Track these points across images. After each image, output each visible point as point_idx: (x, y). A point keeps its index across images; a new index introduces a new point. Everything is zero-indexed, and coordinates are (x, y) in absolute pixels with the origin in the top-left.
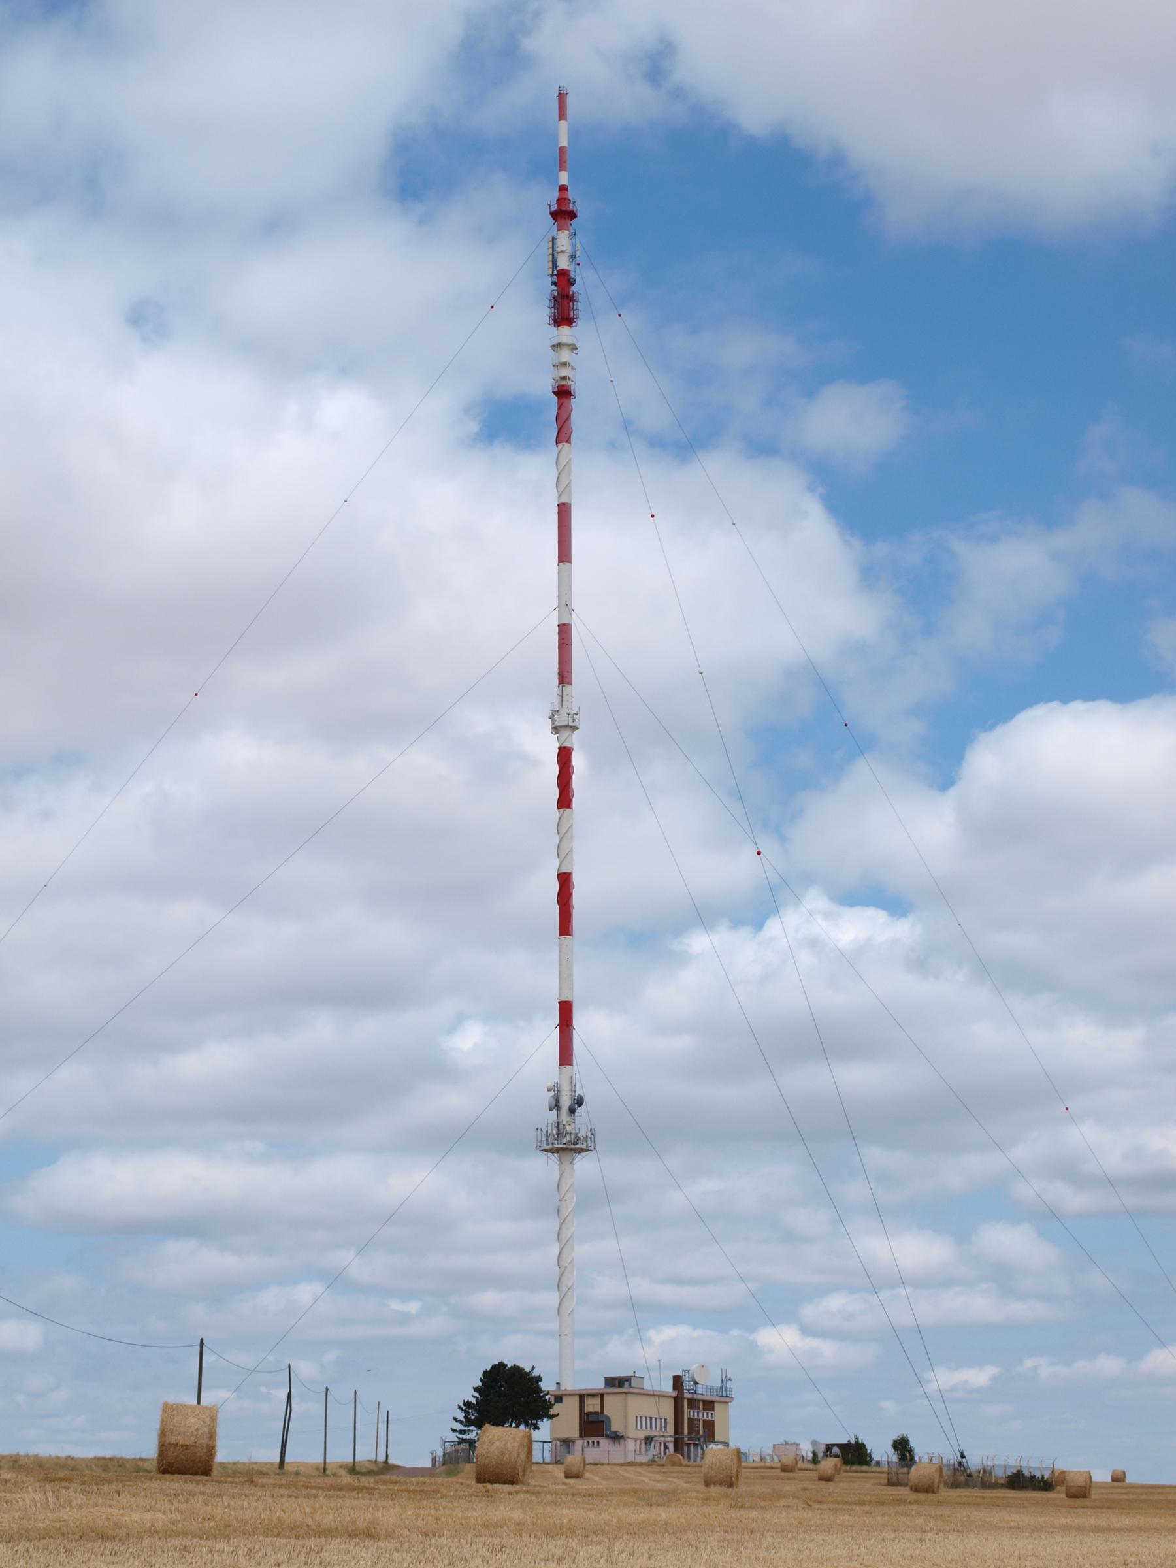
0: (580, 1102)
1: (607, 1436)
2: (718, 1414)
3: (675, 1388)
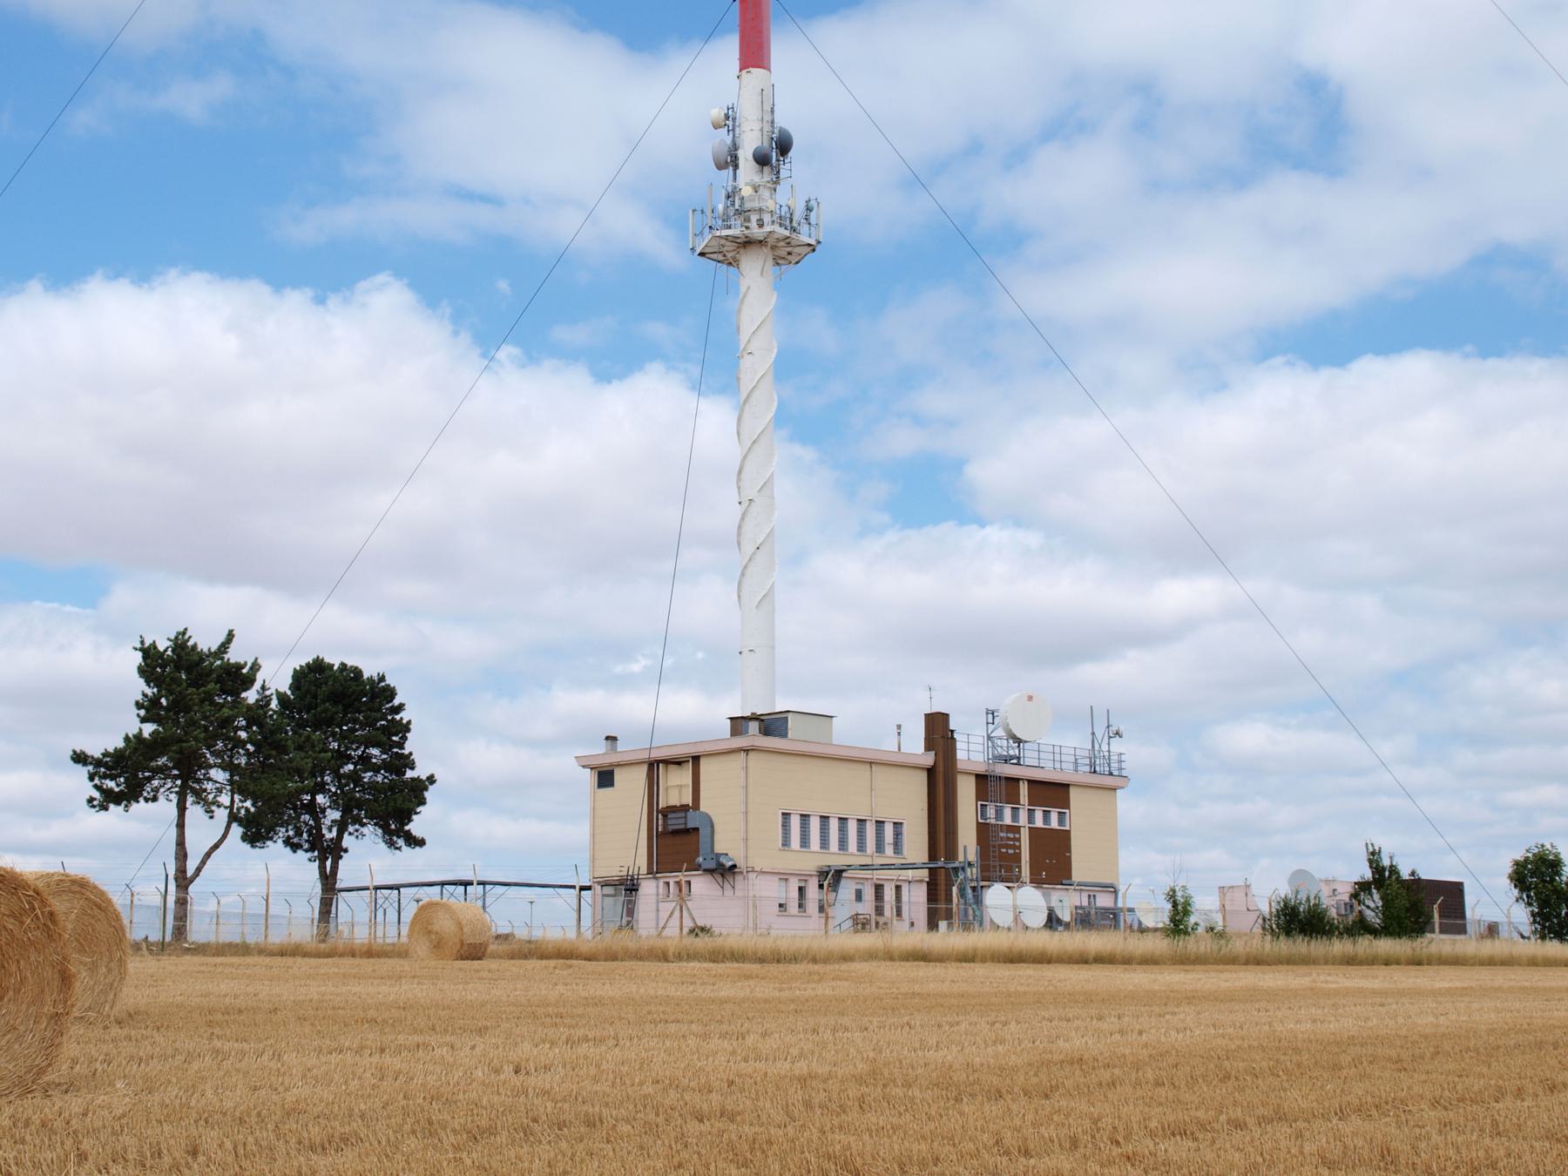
0: (784, 146)
1: (710, 871)
2: (1080, 818)
3: (929, 745)
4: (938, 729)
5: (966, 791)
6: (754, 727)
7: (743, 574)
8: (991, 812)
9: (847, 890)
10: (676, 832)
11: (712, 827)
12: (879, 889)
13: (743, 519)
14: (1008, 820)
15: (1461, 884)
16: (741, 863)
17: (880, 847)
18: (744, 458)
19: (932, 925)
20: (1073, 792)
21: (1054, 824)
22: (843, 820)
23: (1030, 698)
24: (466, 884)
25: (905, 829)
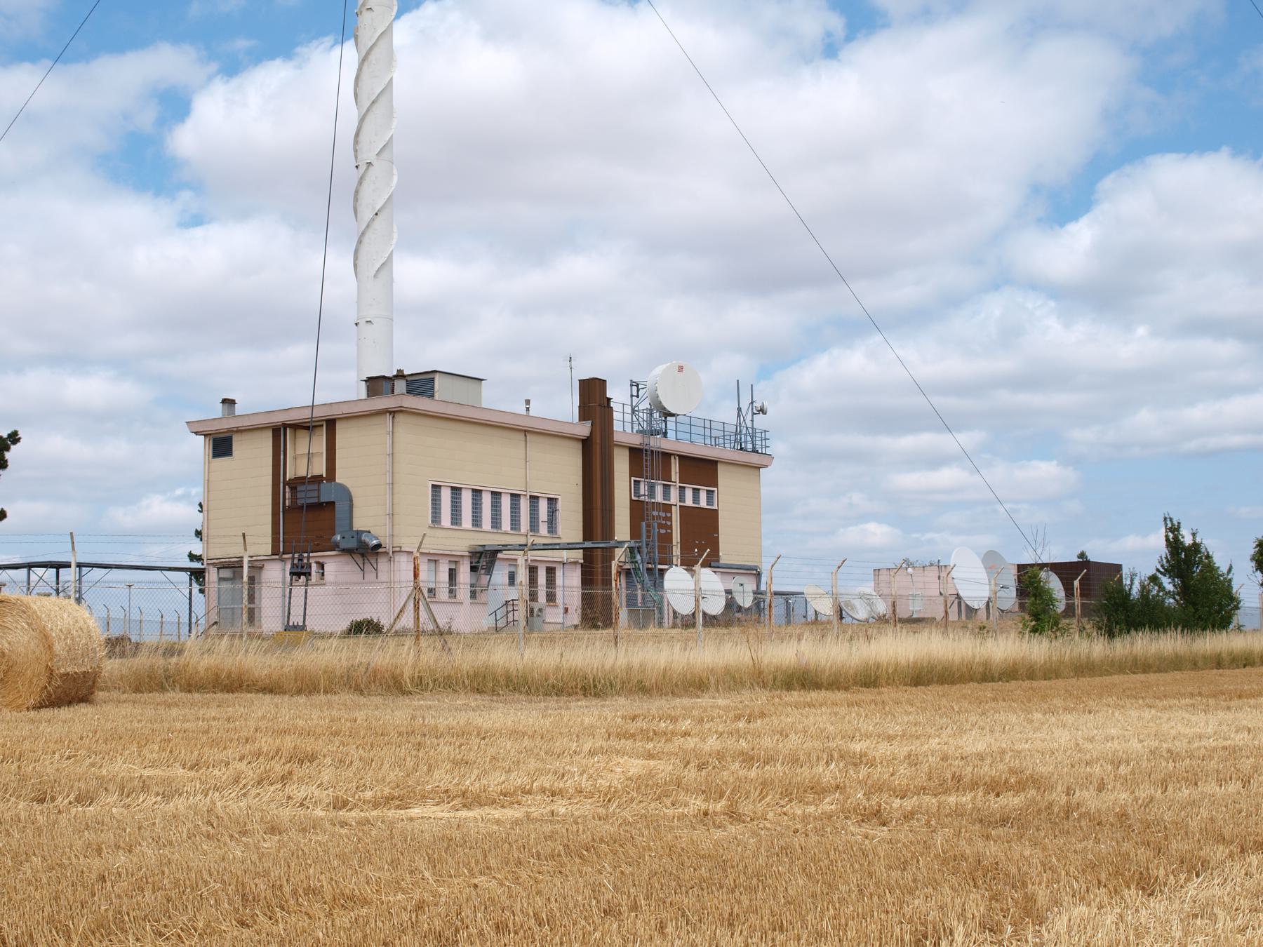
1: (349, 552)
2: (729, 496)
3: (585, 413)
4: (593, 395)
5: (621, 465)
6: (400, 386)
7: (360, 242)
8: (643, 489)
9: (500, 575)
10: (311, 507)
11: (351, 500)
12: (533, 570)
13: (360, 183)
14: (659, 498)
15: (1120, 566)
16: (385, 541)
17: (534, 526)
18: (362, 120)
19: (596, 613)
20: (720, 467)
21: (703, 503)
22: (496, 495)
23: (681, 369)
24: (58, 566)
25: (560, 505)
